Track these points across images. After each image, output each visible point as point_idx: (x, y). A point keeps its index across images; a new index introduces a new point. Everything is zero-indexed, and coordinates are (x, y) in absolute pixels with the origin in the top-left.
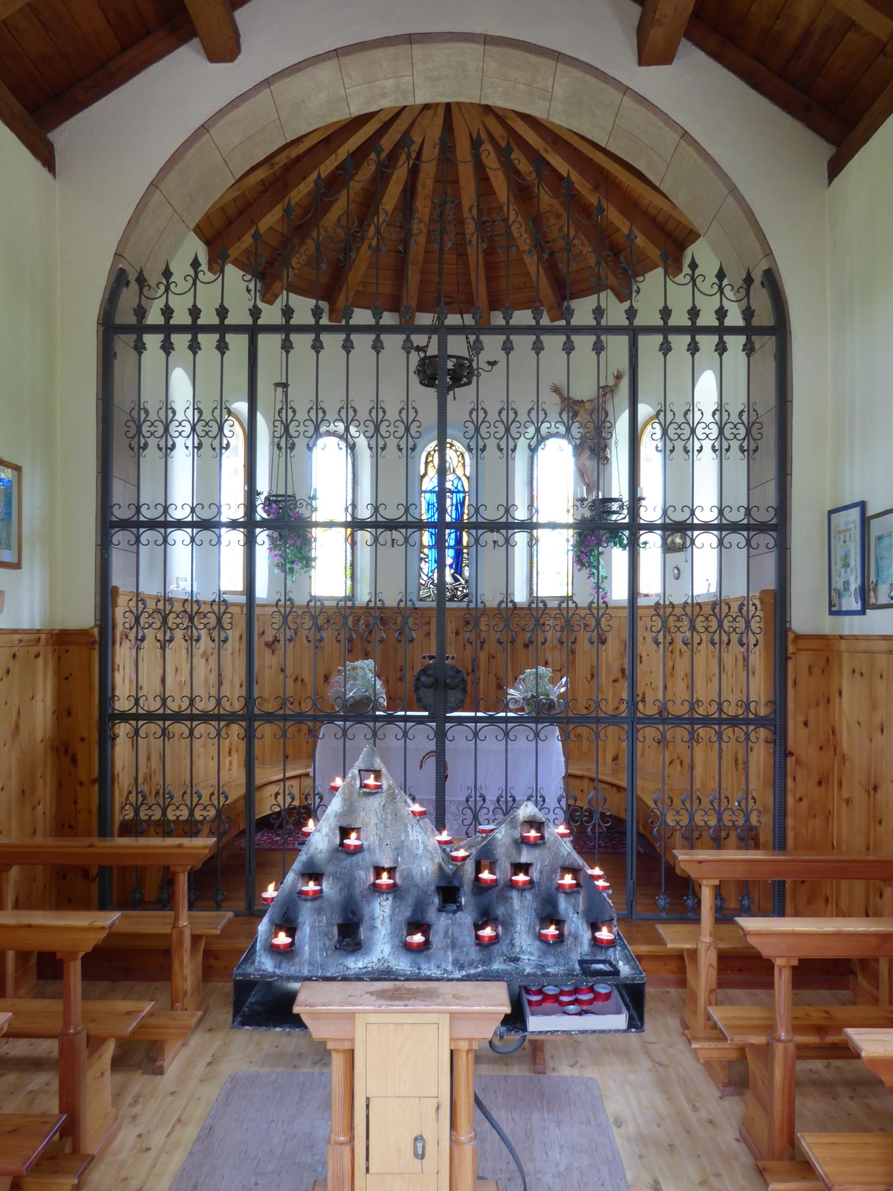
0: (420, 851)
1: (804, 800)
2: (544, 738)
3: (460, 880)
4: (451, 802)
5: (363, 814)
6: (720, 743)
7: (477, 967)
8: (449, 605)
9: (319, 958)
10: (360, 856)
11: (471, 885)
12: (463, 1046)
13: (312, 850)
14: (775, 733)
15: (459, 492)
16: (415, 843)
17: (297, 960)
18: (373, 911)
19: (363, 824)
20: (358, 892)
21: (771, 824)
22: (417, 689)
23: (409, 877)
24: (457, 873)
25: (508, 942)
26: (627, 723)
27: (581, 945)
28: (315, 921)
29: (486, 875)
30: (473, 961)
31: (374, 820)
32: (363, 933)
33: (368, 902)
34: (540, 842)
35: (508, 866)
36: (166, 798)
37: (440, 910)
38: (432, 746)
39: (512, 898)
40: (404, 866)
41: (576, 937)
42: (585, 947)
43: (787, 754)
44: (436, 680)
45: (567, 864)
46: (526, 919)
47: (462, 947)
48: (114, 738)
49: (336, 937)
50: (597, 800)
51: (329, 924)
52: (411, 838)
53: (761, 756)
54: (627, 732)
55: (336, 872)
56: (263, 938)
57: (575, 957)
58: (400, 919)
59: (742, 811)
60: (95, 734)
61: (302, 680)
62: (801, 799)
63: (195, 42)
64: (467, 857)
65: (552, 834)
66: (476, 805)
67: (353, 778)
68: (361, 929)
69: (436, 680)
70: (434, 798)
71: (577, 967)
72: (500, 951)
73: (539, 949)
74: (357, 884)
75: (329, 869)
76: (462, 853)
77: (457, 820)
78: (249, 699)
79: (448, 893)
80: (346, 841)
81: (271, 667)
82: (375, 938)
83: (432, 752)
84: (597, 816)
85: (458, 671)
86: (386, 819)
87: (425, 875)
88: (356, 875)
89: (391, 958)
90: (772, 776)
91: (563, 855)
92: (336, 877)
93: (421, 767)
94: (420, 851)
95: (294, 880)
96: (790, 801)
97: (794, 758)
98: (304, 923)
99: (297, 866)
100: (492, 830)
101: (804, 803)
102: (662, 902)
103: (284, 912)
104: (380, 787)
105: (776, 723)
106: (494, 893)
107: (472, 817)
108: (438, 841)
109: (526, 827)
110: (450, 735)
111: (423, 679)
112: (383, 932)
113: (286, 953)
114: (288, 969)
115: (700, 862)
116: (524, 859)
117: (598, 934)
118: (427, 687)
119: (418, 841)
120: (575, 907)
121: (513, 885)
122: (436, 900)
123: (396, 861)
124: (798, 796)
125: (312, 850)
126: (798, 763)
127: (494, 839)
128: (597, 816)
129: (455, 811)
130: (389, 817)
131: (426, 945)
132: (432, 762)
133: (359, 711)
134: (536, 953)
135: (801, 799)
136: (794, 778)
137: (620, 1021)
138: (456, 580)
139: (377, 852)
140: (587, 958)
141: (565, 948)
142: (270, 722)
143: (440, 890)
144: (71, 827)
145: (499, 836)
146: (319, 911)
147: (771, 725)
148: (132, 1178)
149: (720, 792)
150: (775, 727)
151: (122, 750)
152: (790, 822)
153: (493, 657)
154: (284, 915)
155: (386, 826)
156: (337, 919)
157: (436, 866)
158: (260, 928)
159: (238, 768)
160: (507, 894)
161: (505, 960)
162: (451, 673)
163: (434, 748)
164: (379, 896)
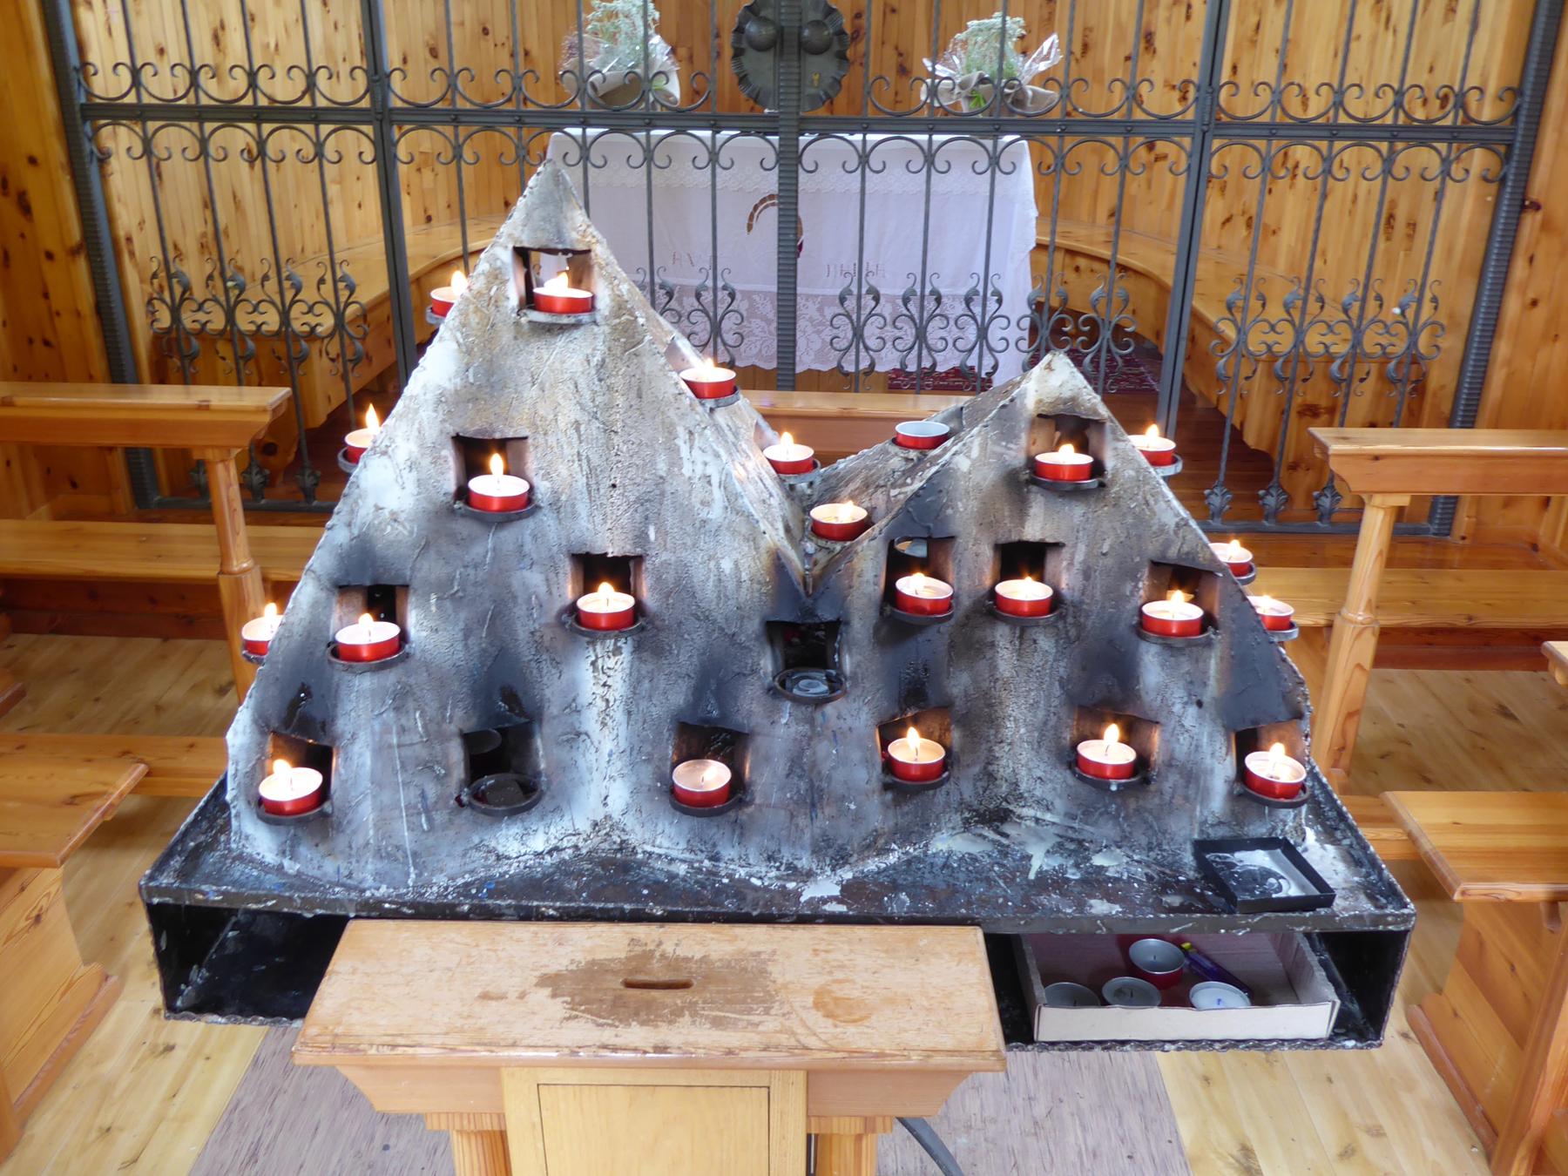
0: (716, 513)
1: (1541, 305)
2: (1008, 168)
3: (842, 600)
4: (808, 297)
5: (531, 393)
6: (1385, 183)
7: (884, 851)
9: (406, 837)
10: (529, 525)
11: (872, 615)
13: (365, 512)
14: (1506, 159)
16: (698, 485)
17: (341, 841)
18: (573, 685)
19: (534, 425)
20: (522, 634)
21: (1458, 354)
22: (738, 53)
23: (681, 588)
24: (824, 581)
25: (976, 769)
26: (1193, 135)
27: (1205, 795)
28: (386, 730)
29: (916, 586)
30: (877, 834)
31: (569, 413)
32: (544, 751)
33: (556, 663)
35: (987, 553)
36: (230, 285)
37: (779, 690)
38: (770, 183)
39: (993, 645)
40: (664, 556)
41: (1193, 776)
42: (1217, 800)
43: (1525, 205)
44: (781, 32)
45: (1172, 554)
46: (1034, 706)
47: (843, 798)
48: (103, 158)
49: (459, 772)
50: (1109, 302)
51: (434, 735)
52: (687, 470)
53: (1465, 207)
54: (1190, 156)
55: (452, 581)
56: (243, 767)
57: (1183, 831)
58: (655, 711)
59: (1406, 325)
60: (56, 152)
61: (527, 53)
62: (1534, 303)
64: (863, 525)
65: (1127, 460)
66: (859, 307)
67: (496, 276)
68: (539, 742)
69: (781, 32)
70: (774, 289)
71: (1188, 858)
72: (955, 798)
73: (1072, 797)
74: (520, 611)
75: (429, 569)
76: (844, 513)
77: (819, 332)
78: (377, 76)
79: (802, 637)
80: (478, 485)
81: (462, 24)
82: (582, 763)
83: (771, 197)
84: (1106, 334)
85: (830, 11)
86: (609, 406)
87: (731, 585)
88: (516, 584)
89: (630, 822)
90: (1481, 254)
91: (1162, 529)
92: (451, 595)
93: (750, 227)
94: (716, 513)
95: (315, 604)
96: (1513, 305)
97: (1539, 216)
98: (354, 737)
99: (322, 560)
100: (938, 441)
101: (1540, 313)
102: (1217, 499)
103: (290, 696)
104: (588, 306)
105: (1514, 139)
106: (937, 639)
107: (850, 334)
108: (774, 463)
109: (1041, 437)
110: (807, 161)
111: (752, 28)
112: (607, 746)
113: (312, 818)
114: (318, 866)
115: (1377, 458)
116: (1034, 529)
117: (1254, 762)
118: (760, 48)
119: (708, 479)
120: (1193, 686)
121: (994, 608)
122: (767, 663)
123: (642, 537)
124: (1531, 295)
125: (365, 512)
126: (1546, 226)
127: (946, 472)
128: (1106, 334)
129: (816, 315)
130: (620, 400)
131: (737, 790)
132: (771, 216)
133: (625, 106)
134: (1059, 804)
135: (1534, 303)
136: (1531, 259)
137: (1313, 1017)
139: (583, 509)
140: (1217, 833)
141: (1152, 802)
142: (423, 125)
143: (775, 631)
144: (47, 343)
145: (963, 464)
146: (401, 699)
147: (1499, 142)
148: (121, 1130)
149: (1366, 287)
150: (1510, 147)
151: (126, 182)
152: (1502, 349)
153: (893, 11)
154: (294, 704)
155: (609, 431)
156: (459, 718)
157: (765, 559)
158: (229, 736)
159: (414, 224)
160: (978, 634)
161: (966, 822)
162: (813, 16)
163: (774, 188)
164: (592, 643)
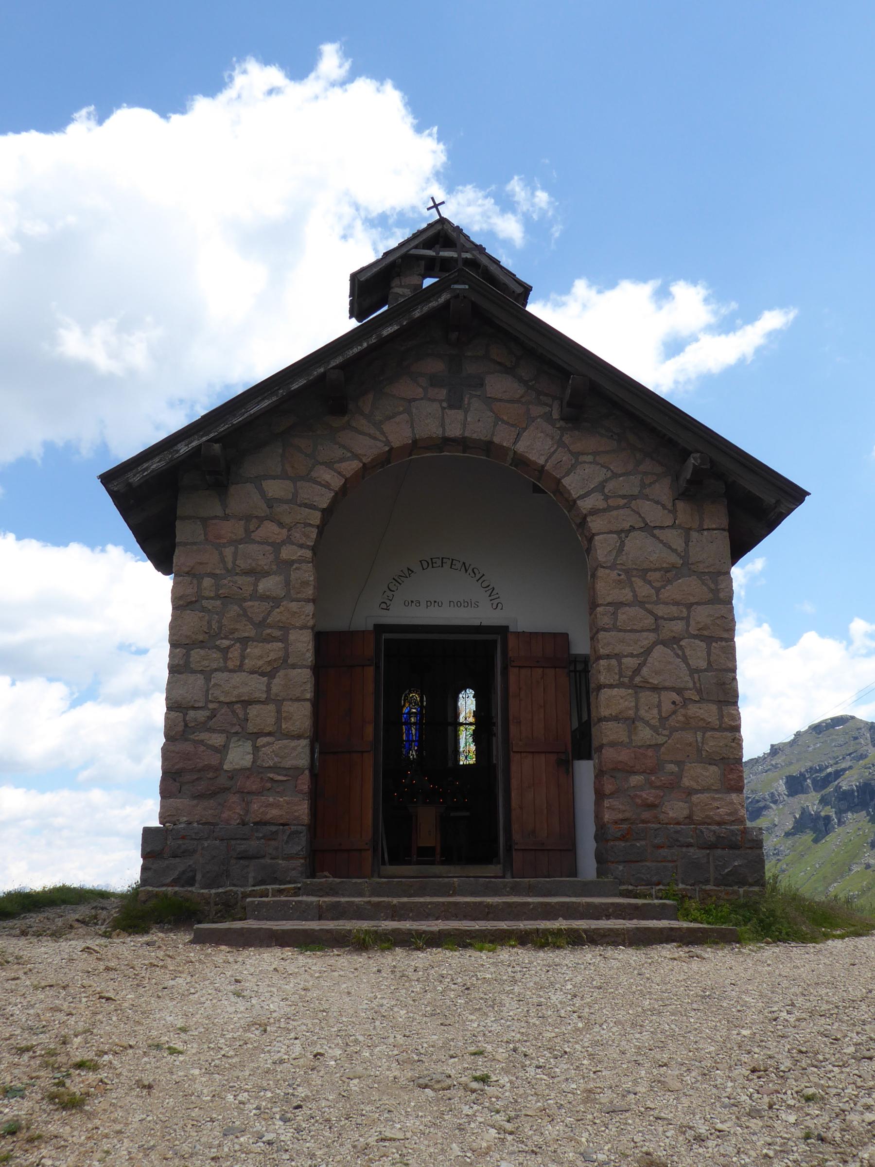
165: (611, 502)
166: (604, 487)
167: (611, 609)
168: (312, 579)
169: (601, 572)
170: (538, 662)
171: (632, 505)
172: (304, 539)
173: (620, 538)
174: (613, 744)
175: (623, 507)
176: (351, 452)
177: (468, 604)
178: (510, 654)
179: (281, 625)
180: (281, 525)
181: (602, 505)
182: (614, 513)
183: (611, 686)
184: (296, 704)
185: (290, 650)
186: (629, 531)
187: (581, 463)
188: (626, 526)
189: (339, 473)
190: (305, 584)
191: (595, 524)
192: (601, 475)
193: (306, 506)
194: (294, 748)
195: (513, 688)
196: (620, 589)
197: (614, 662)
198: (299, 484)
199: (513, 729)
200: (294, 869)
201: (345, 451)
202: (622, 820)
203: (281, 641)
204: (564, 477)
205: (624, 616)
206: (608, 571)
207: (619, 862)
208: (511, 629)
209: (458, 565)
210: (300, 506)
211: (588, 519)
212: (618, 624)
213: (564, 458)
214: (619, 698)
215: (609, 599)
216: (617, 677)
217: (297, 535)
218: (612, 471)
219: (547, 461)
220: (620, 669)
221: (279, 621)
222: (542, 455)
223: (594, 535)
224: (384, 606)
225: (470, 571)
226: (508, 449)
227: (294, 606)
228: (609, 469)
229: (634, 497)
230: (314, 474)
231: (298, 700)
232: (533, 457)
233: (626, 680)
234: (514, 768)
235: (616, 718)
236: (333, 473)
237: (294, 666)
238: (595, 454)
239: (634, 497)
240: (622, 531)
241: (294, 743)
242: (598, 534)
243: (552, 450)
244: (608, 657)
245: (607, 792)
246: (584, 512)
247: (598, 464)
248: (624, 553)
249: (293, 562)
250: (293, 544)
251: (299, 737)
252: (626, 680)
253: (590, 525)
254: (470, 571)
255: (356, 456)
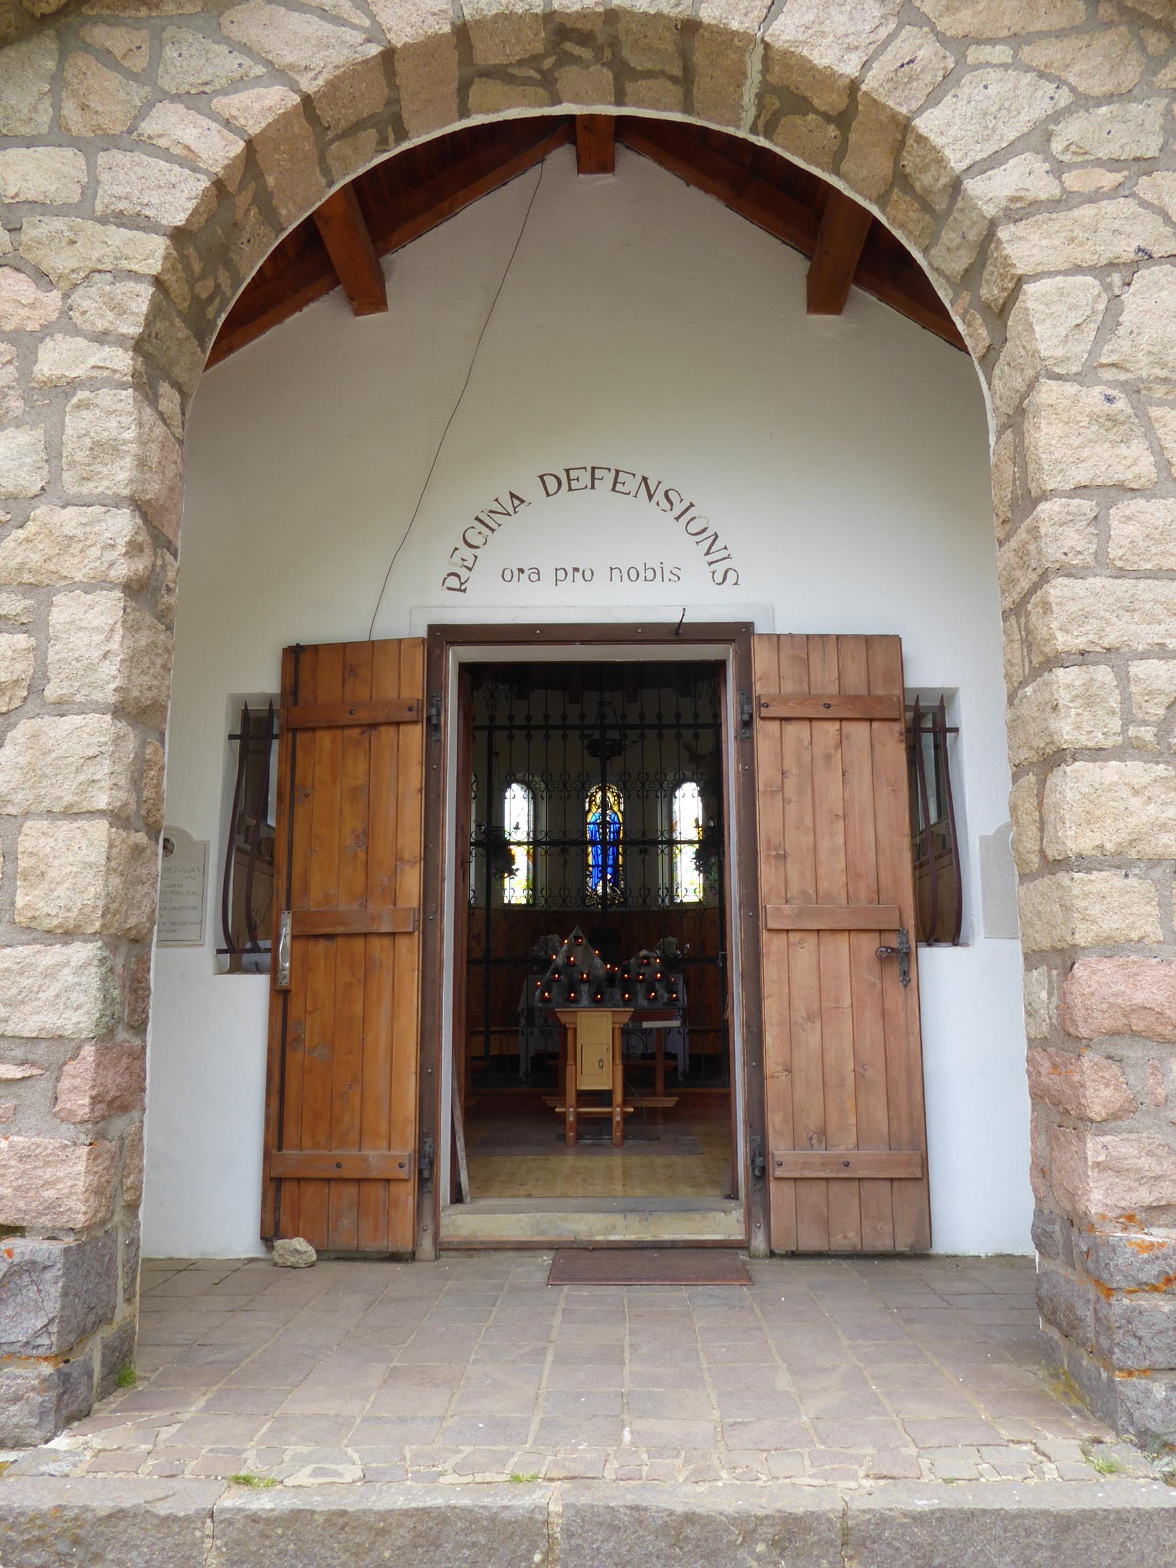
8: (610, 909)
12: (617, 1026)
15: (615, 823)
34: (648, 964)
58: (564, 82)
63: (340, 287)
138: (614, 891)
165: (1072, 180)
166: (1049, 137)
167: (1087, 506)
168: (129, 435)
169: (1048, 392)
170: (828, 706)
171: (1138, 190)
172: (110, 316)
173: (1108, 287)
174: (1110, 948)
175: (1114, 193)
176: (269, 63)
177: (654, 574)
178: (758, 689)
179: (27, 578)
180: (42, 278)
181: (1044, 187)
182: (1086, 212)
183: (1097, 754)
184: (66, 828)
185: (52, 657)
186: (1134, 267)
187: (976, 67)
188: (1125, 250)
189: (227, 123)
190: (104, 449)
191: (1022, 247)
192: (1039, 101)
193: (121, 220)
194: (50, 974)
195: (765, 771)
196: (1113, 444)
197: (1103, 674)
198: (102, 158)
199: (767, 874)
200: (16, 1399)
201: (247, 62)
202: (1150, 1208)
203: (24, 628)
204: (920, 111)
205: (1131, 529)
206: (1071, 388)
207: (1150, 1371)
208: (759, 629)
209: (632, 484)
210: (103, 221)
211: (1003, 233)
212: (1114, 552)
213: (921, 53)
214: (1125, 792)
215: (1081, 475)
216: (1116, 724)
217: (90, 305)
218: (1073, 89)
219: (866, 66)
220: (1126, 699)
221: (20, 569)
222: (850, 49)
223: (1020, 281)
224: (453, 582)
225: (659, 496)
226: (748, 38)
227: (69, 519)
228: (1060, 82)
229: (1144, 165)
230: (148, 127)
231: (71, 814)
232: (822, 57)
233: (1147, 733)
234: (770, 971)
235: (1117, 861)
236: (206, 122)
237: (61, 708)
238: (1017, 40)
239: (1144, 165)
240: (1112, 266)
241: (55, 954)
242: (1036, 277)
243: (883, 33)
244: (1083, 657)
245: (1096, 1110)
246: (990, 211)
247: (1029, 69)
248: (1121, 331)
249: (74, 385)
250: (77, 332)
251: (68, 935)
252: (1147, 733)
253: (1008, 250)
254: (659, 496)
255: (279, 74)
